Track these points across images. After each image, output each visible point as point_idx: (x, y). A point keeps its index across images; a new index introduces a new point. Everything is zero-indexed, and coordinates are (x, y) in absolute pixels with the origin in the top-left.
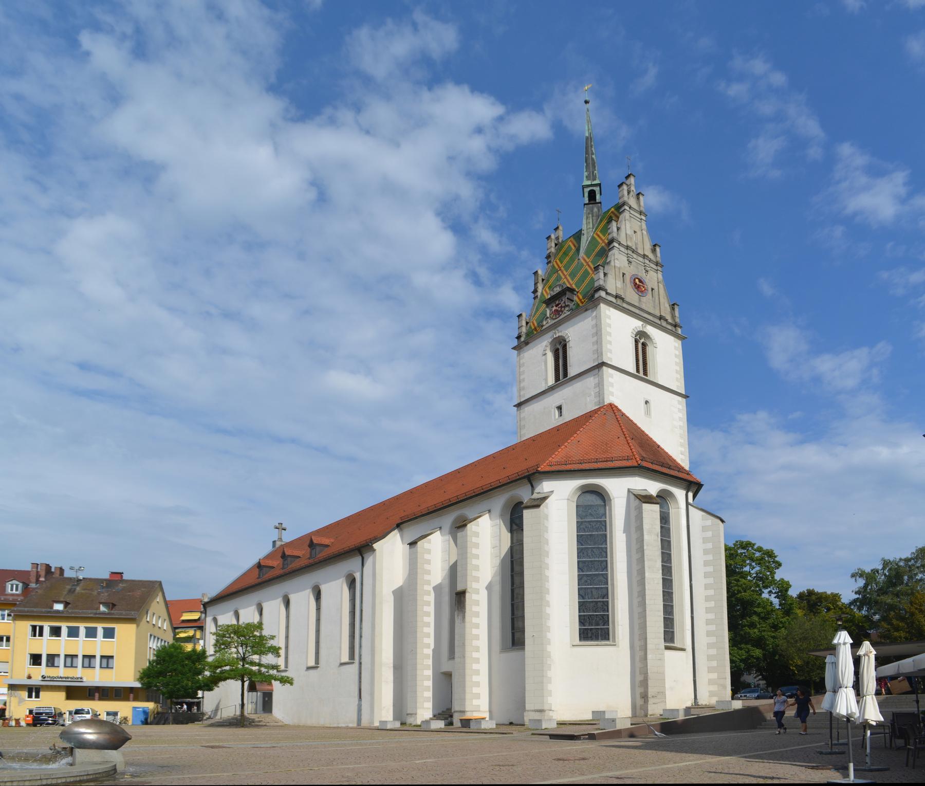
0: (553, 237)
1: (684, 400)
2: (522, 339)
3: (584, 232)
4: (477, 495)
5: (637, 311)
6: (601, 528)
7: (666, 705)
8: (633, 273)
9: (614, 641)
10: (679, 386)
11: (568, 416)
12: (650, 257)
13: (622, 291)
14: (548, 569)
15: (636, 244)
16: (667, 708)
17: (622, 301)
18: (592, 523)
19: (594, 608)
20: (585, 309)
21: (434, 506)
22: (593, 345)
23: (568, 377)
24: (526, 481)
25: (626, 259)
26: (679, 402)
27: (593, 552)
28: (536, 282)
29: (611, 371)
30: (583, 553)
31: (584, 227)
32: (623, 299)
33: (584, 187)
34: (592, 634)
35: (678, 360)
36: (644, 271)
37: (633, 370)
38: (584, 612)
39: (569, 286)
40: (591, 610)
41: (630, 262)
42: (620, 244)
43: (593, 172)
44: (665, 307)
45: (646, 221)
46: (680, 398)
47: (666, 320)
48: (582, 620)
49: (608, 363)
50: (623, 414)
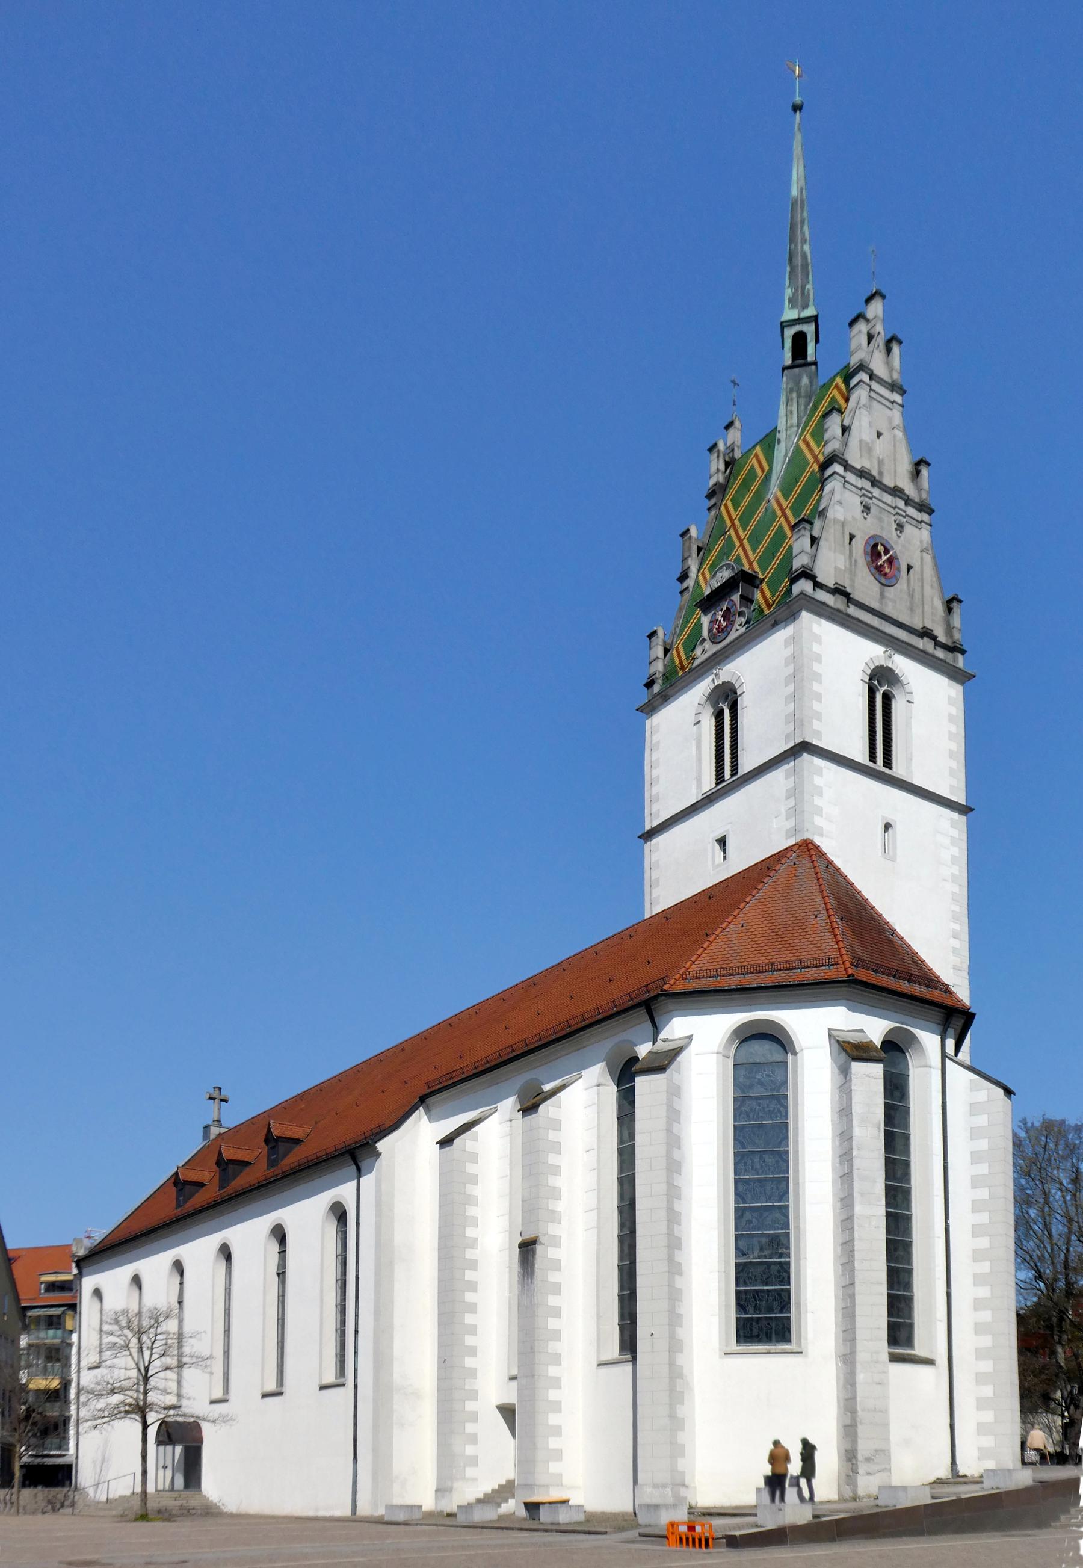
0: (721, 446)
1: (964, 819)
2: (656, 688)
3: (782, 436)
4: (558, 1040)
5: (875, 621)
6: (779, 1111)
7: (890, 1477)
8: (872, 533)
9: (799, 1344)
10: (953, 787)
11: (741, 859)
12: (907, 492)
13: (847, 575)
14: (679, 1198)
15: (880, 462)
16: (894, 1484)
17: (845, 600)
18: (761, 1102)
19: (765, 1277)
20: (773, 622)
21: (509, 1049)
22: (658, 795)
23: (739, 775)
24: (643, 1012)
25: (857, 500)
26: (953, 824)
27: (764, 1162)
28: (686, 555)
29: (818, 761)
30: (745, 1164)
31: (781, 424)
32: (846, 595)
33: (783, 326)
34: (761, 1329)
35: (954, 729)
36: (895, 526)
37: (861, 755)
38: (745, 1284)
39: (746, 568)
40: (759, 1281)
41: (867, 509)
42: (847, 466)
43: (803, 287)
44: (933, 607)
45: (903, 406)
46: (955, 815)
47: (934, 638)
48: (743, 1301)
49: (815, 743)
50: (829, 864)
